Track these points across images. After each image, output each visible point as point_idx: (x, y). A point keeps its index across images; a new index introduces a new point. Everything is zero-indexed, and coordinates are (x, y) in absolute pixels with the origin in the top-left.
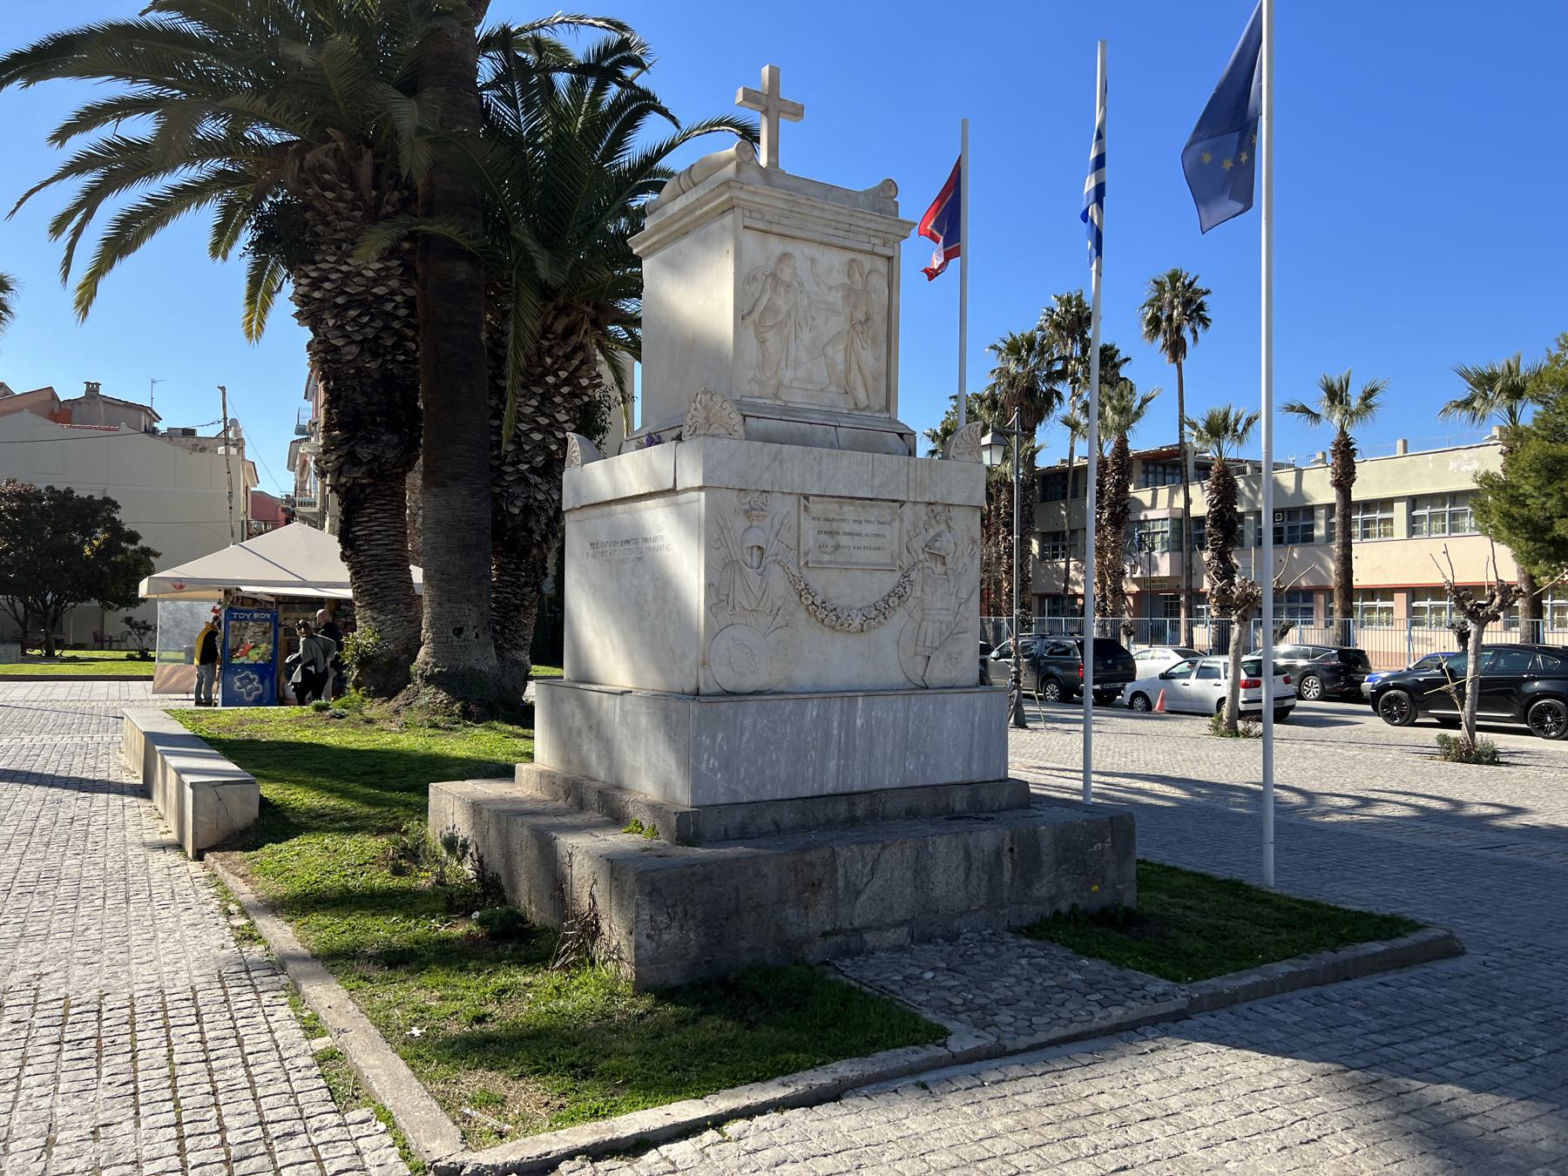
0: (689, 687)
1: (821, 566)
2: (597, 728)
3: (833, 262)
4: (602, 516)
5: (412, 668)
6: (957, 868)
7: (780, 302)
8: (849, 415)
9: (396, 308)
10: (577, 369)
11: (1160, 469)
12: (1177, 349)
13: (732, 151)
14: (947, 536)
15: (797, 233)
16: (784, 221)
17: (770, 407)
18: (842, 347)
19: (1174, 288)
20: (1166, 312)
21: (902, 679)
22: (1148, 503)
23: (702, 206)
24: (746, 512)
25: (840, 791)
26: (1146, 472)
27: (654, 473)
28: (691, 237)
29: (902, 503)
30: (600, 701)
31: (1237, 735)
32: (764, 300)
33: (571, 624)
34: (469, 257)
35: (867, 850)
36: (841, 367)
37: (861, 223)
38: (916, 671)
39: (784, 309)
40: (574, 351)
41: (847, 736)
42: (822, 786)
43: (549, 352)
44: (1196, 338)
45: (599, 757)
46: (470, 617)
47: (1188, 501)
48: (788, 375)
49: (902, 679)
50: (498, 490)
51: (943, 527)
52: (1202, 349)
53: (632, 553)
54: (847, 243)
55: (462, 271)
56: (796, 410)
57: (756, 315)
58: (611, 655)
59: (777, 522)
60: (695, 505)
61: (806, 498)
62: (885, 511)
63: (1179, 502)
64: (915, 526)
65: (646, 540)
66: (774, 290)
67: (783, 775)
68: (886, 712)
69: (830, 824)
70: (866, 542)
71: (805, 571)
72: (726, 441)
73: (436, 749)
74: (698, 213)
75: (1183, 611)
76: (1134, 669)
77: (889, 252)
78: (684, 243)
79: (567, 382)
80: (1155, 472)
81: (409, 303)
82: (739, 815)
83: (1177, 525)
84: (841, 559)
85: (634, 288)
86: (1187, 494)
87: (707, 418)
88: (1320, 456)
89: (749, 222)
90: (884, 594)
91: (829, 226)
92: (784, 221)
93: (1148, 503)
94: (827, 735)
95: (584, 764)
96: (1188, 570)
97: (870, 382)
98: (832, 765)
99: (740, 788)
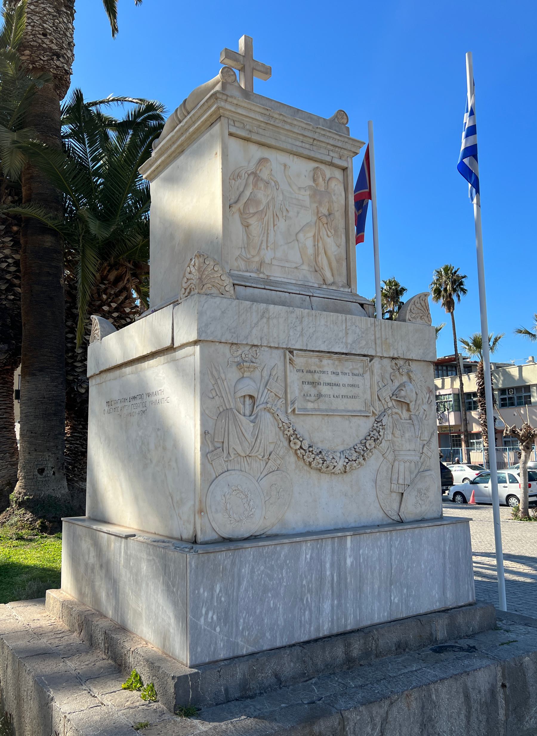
0: (187, 534)
1: (306, 413)
2: (106, 566)
3: (302, 168)
4: (115, 379)
5: (11, 496)
6: (459, 713)
7: (260, 195)
8: (319, 288)
9: (8, 266)
10: (123, 302)
11: (445, 368)
12: (449, 305)
13: (219, 76)
14: (410, 386)
15: (273, 142)
16: (261, 131)
17: (254, 279)
18: (311, 234)
19: (446, 274)
20: (444, 286)
21: (381, 515)
22: (440, 386)
23: (194, 123)
24: (238, 364)
25: (335, 631)
26: (437, 370)
27: (155, 335)
28: (187, 152)
29: (372, 357)
30: (109, 541)
31: (530, 519)
32: (247, 194)
33: (92, 471)
34: (53, 232)
35: (375, 709)
36: (310, 251)
37: (322, 139)
38: (392, 507)
39: (264, 202)
40: (121, 292)
41: (339, 575)
42: (318, 629)
43: (105, 291)
44: (459, 299)
45: (108, 595)
46: (50, 462)
47: (462, 384)
48: (268, 255)
49: (381, 515)
50: (71, 378)
51: (405, 379)
52: (465, 304)
53: (140, 405)
54: (312, 154)
55: (48, 241)
56: (276, 283)
57: (241, 204)
58: (121, 498)
59: (265, 374)
60: (191, 359)
61: (291, 352)
62: (357, 365)
63: (457, 385)
64: (383, 378)
65: (149, 395)
66: (255, 185)
67: (281, 622)
68: (373, 549)
69: (329, 670)
70: (344, 391)
71: (292, 418)
72: (218, 300)
73: (14, 559)
74: (191, 130)
75: (463, 443)
76: (452, 478)
77: (344, 164)
78: (182, 159)
79: (116, 310)
80: (442, 370)
81: (17, 263)
82: (240, 671)
83: (456, 397)
84: (323, 406)
85: (145, 198)
86: (461, 381)
87: (200, 279)
88: (530, 358)
89: (233, 130)
90: (362, 438)
91: (296, 139)
92: (261, 131)
93: (440, 386)
94: (321, 579)
95: (96, 600)
96: (465, 421)
97: (334, 264)
98: (327, 606)
99: (239, 640)
